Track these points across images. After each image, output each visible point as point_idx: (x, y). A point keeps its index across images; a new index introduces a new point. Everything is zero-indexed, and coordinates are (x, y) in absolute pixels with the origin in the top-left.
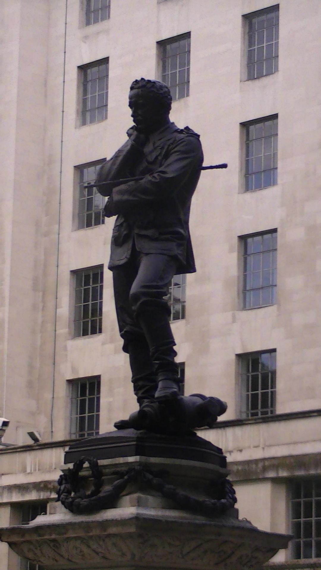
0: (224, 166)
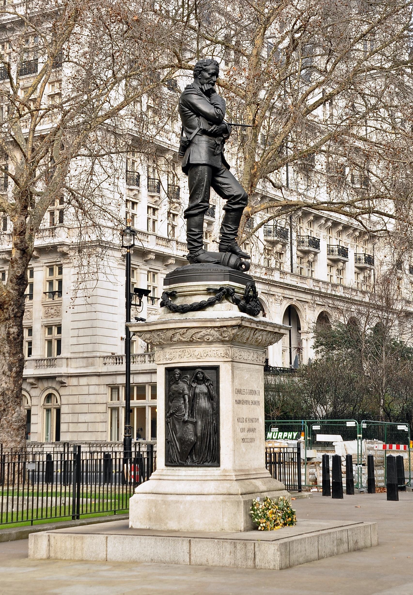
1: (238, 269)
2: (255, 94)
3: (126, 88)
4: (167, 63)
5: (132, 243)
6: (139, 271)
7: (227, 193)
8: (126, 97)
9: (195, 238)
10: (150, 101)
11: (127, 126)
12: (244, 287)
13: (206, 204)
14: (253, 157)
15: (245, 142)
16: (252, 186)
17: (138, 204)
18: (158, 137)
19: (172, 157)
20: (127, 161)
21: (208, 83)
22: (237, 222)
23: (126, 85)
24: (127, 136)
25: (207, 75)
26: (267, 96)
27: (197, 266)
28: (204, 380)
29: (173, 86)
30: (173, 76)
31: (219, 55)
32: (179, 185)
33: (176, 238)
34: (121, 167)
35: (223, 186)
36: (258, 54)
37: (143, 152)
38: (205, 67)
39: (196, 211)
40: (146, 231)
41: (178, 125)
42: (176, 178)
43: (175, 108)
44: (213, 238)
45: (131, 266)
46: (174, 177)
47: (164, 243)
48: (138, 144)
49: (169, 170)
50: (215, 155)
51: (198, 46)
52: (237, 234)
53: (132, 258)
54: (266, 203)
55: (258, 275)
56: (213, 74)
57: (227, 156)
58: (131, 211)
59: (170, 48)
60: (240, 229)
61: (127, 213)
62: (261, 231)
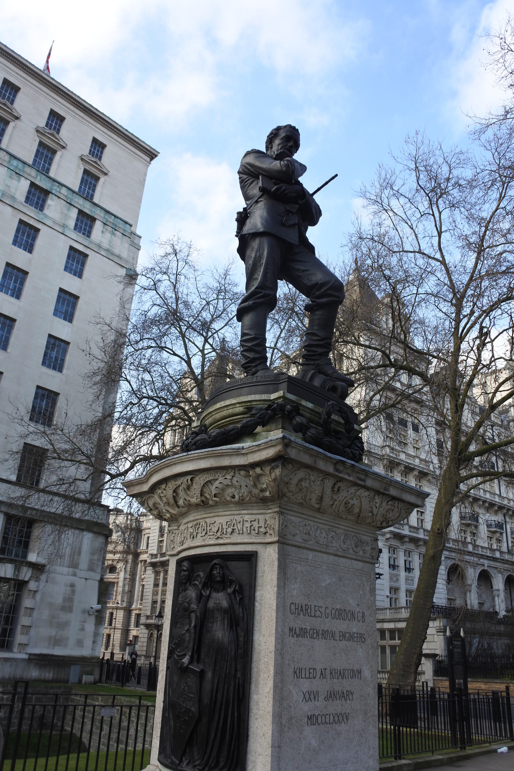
0: (336, 175)
28: (223, 583)
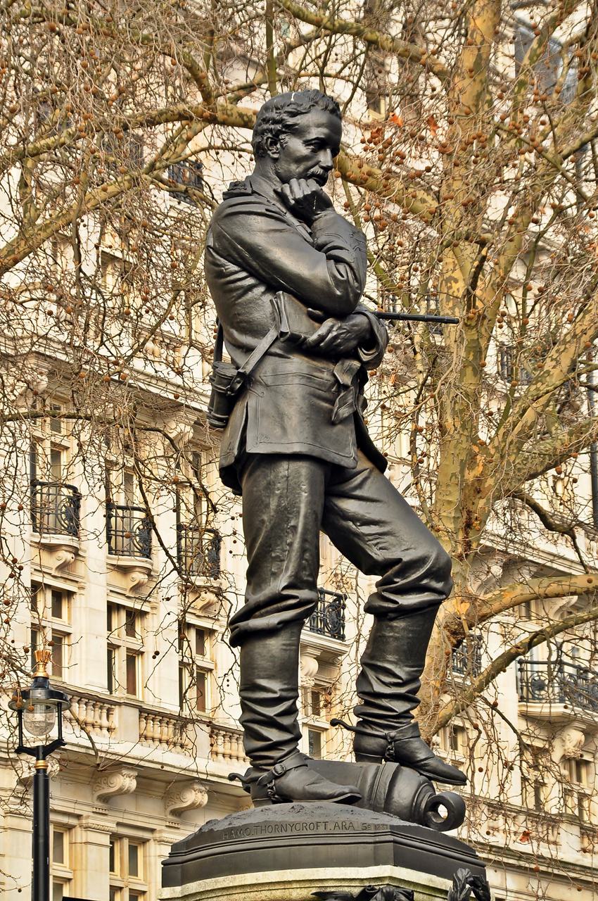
1: (425, 821)
2: (473, 208)
3: (23, 195)
4: (162, 105)
5: (54, 734)
6: (80, 835)
7: (378, 555)
8: (24, 225)
9: (271, 712)
10: (108, 240)
11: (29, 327)
12: (447, 884)
13: (304, 594)
14: (469, 426)
15: (438, 375)
16: (468, 525)
17: (77, 600)
18: (138, 364)
19: (189, 432)
20: (33, 447)
21: (305, 176)
22: (415, 653)
23: (23, 184)
24: (32, 362)
25: (298, 146)
26: (511, 211)
27: (278, 812)
29: (188, 184)
30: (188, 151)
31: (346, 72)
32: (215, 525)
33: (208, 713)
34: (12, 470)
35: (365, 530)
36: (481, 66)
37: (88, 418)
38: (291, 121)
39: (273, 620)
40: (102, 691)
41: (205, 322)
42: (204, 504)
43: (195, 261)
44: (336, 712)
45: (52, 817)
46: (197, 499)
47: (168, 732)
48: (71, 388)
49: (181, 478)
50: (333, 424)
51: (270, 42)
52: (418, 696)
53: (54, 789)
54: (523, 585)
55: (499, 840)
56: (320, 145)
57: (375, 427)
58: (52, 623)
59: (174, 50)
60: (428, 679)
61: (36, 629)
62: (506, 683)
